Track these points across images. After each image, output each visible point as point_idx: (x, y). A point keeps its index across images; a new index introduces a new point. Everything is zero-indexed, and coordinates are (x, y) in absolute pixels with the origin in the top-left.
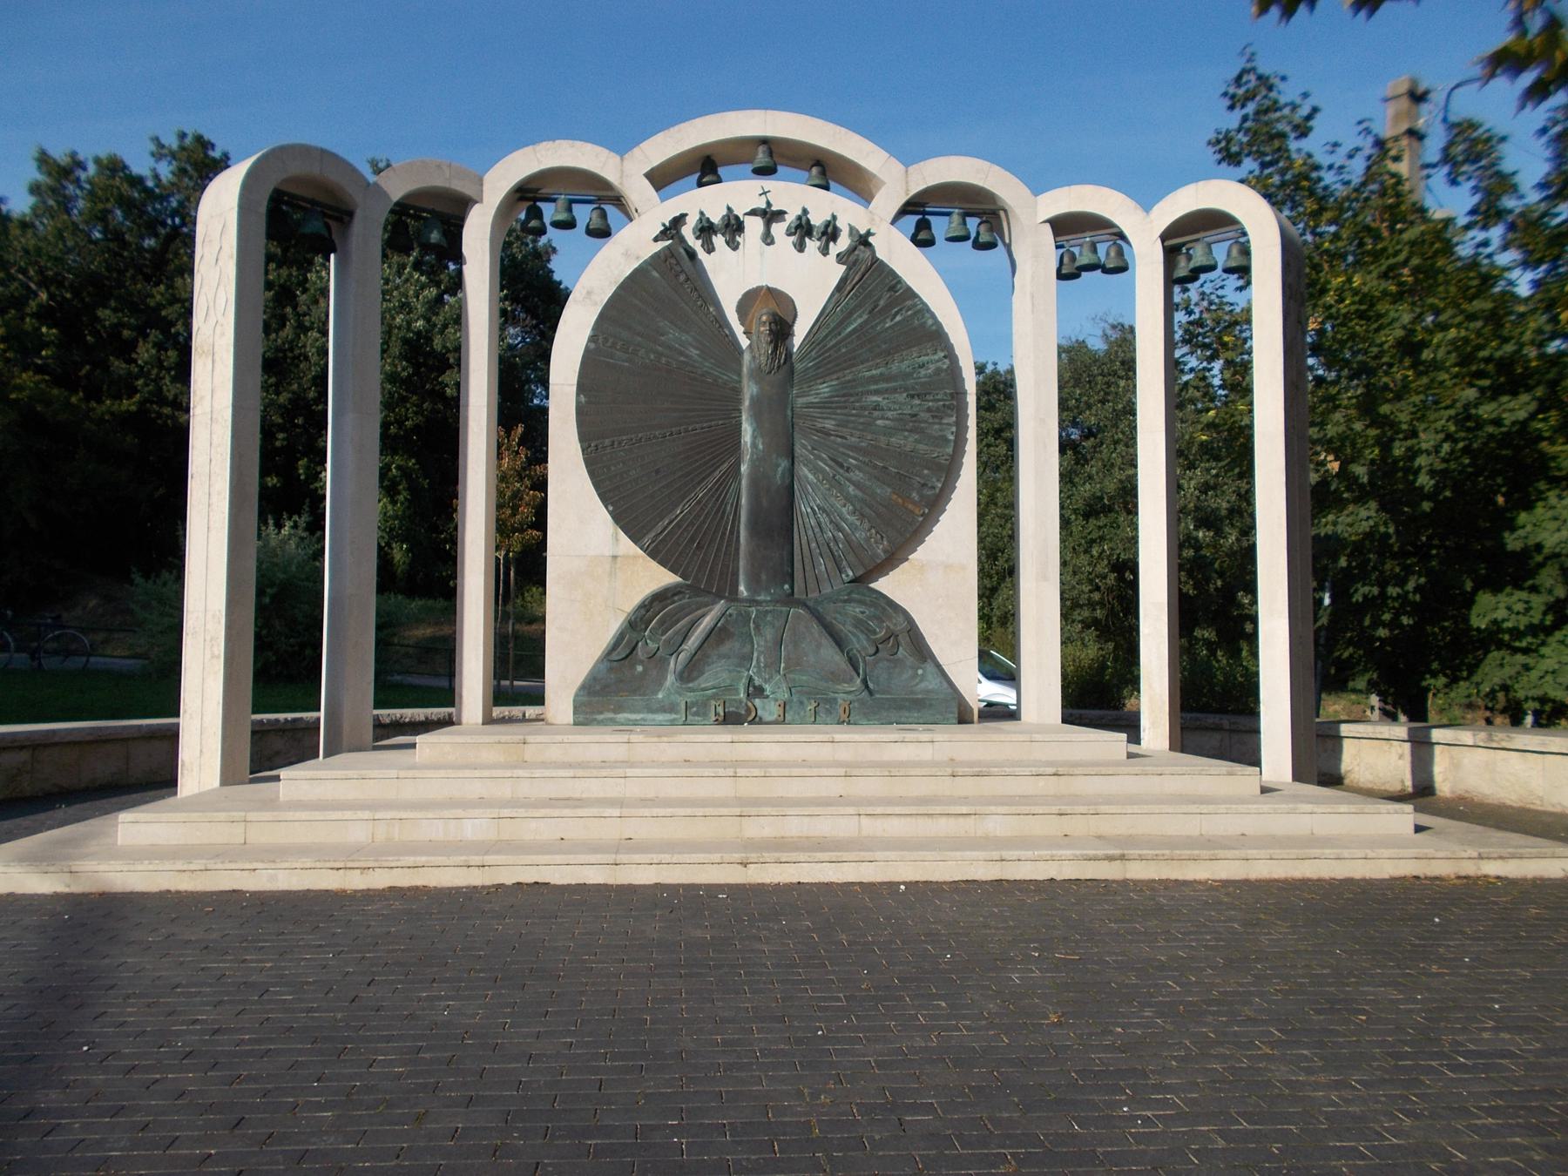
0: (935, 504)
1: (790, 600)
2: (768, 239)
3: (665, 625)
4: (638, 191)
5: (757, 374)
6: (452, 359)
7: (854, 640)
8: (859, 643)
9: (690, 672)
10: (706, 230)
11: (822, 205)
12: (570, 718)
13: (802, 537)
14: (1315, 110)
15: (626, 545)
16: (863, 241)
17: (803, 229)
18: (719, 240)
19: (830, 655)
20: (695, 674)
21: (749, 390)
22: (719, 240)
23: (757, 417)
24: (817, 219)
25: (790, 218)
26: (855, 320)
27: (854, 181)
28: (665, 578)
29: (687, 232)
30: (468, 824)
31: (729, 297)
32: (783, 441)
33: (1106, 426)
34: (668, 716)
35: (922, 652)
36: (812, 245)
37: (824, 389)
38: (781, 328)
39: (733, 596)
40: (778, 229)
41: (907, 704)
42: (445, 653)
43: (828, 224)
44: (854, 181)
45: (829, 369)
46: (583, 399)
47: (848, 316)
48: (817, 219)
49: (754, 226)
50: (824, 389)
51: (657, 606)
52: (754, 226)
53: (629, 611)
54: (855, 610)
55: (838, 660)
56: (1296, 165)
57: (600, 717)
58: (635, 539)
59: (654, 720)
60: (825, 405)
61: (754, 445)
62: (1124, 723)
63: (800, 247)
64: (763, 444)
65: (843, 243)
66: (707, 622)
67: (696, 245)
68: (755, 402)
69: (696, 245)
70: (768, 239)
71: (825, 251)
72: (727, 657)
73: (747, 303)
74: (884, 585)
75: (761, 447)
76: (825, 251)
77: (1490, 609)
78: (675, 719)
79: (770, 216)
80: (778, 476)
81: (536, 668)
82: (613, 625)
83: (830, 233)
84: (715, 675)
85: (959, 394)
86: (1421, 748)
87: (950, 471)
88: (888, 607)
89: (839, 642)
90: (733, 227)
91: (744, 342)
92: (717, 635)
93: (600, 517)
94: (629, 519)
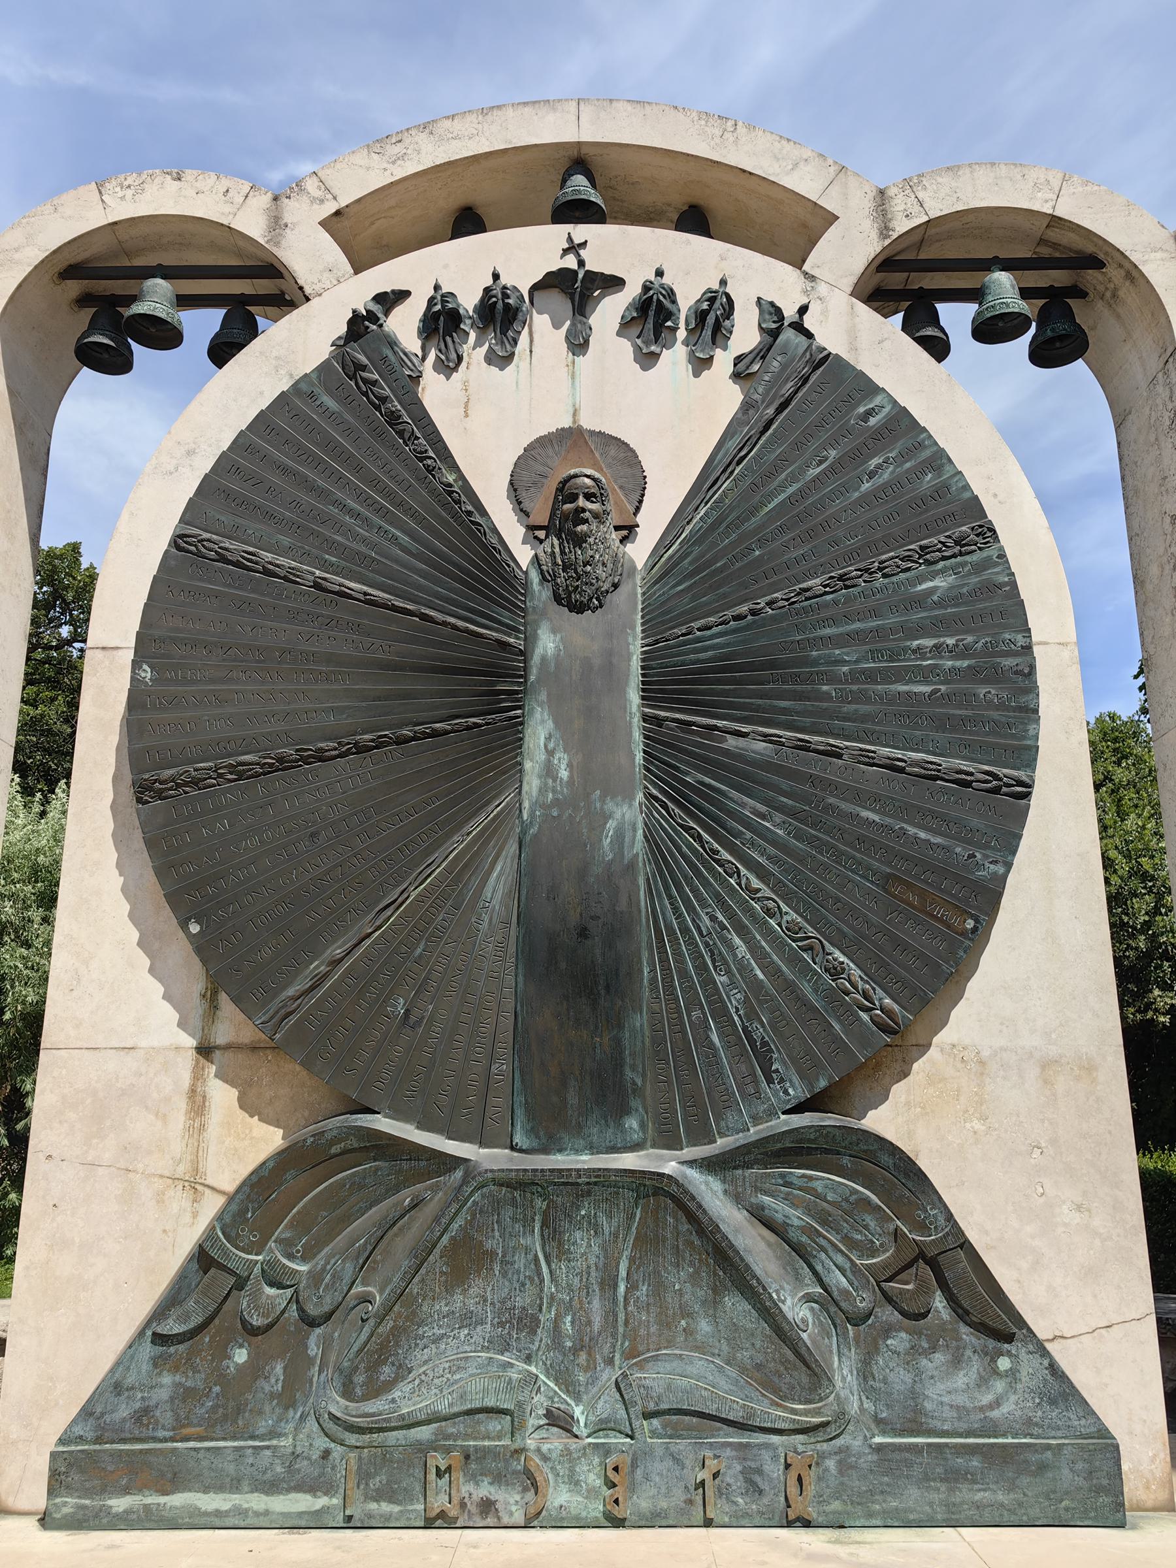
7: (378, 224)
12: (36, 1496)
14: (1136, 677)
20: (387, 1371)
22: (474, 350)
25: (632, 291)
26: (782, 487)
33: (143, 1398)
34: (302, 1502)
41: (975, 1463)
43: (711, 297)
45: (725, 596)
46: (147, 673)
53: (230, 1187)
57: (119, 1504)
59: (267, 1513)
61: (549, 771)
63: (647, 360)
64: (570, 765)
71: (701, 364)
72: (468, 1320)
75: (564, 774)
76: (701, 364)
78: (324, 1510)
80: (606, 842)
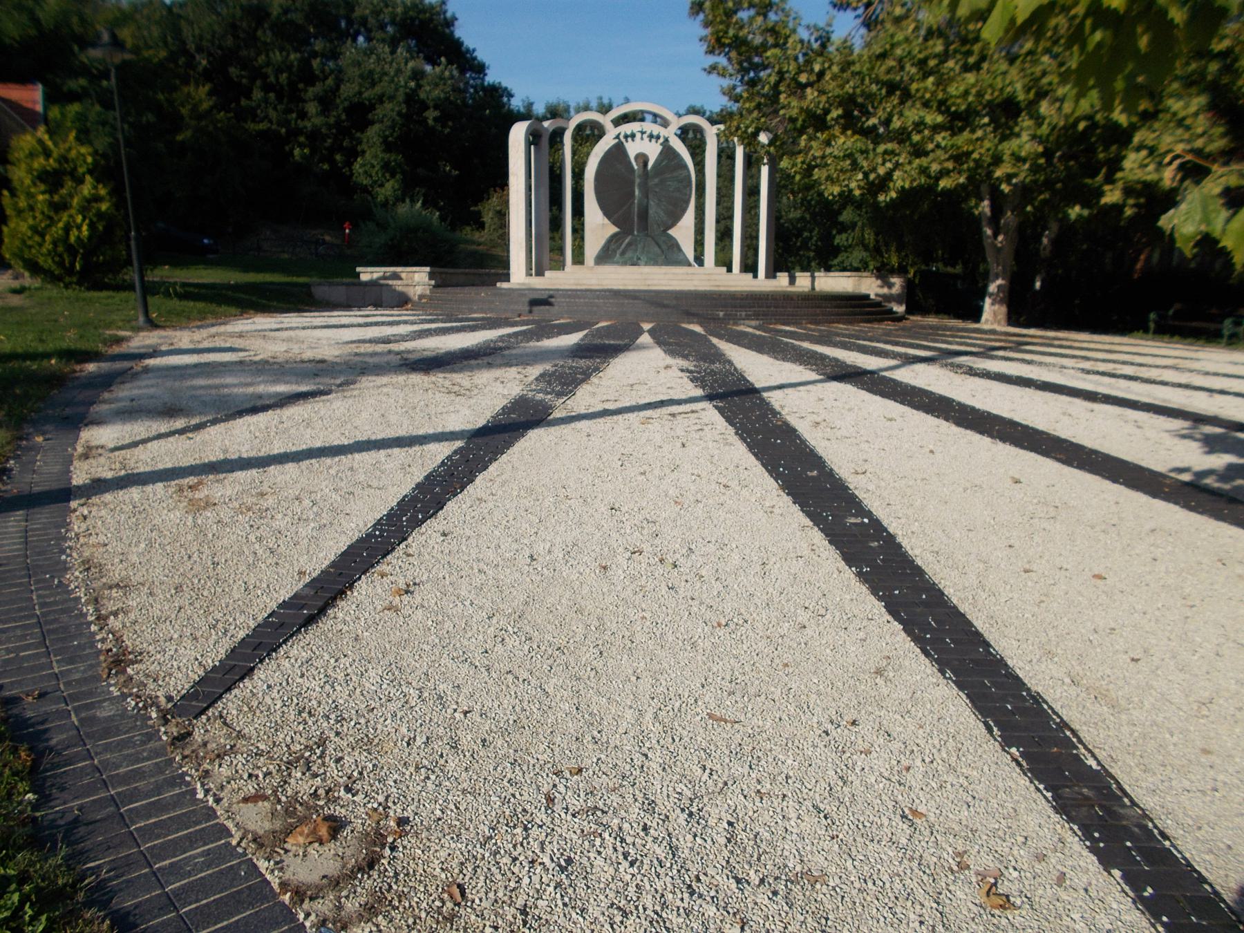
0: (684, 211)
1: (647, 235)
2: (642, 139)
3: (616, 242)
4: (609, 126)
5: (639, 176)
6: (562, 168)
8: (664, 247)
9: (623, 253)
10: (626, 137)
11: (656, 129)
13: (650, 220)
15: (606, 221)
16: (666, 140)
17: (651, 136)
18: (629, 139)
19: (657, 249)
21: (637, 181)
22: (629, 139)
23: (639, 189)
24: (655, 133)
25: (648, 132)
27: (665, 124)
28: (616, 230)
29: (621, 137)
30: (416, 275)
31: (632, 154)
32: (646, 193)
35: (680, 250)
36: (654, 140)
37: (656, 180)
38: (646, 164)
39: (633, 235)
40: (645, 136)
42: (561, 250)
44: (665, 124)
47: (662, 161)
48: (655, 133)
49: (638, 136)
50: (656, 180)
51: (613, 247)
52: (638, 136)
54: (663, 238)
55: (659, 251)
56: (857, 50)
58: (609, 218)
60: (656, 185)
62: (178, 372)
65: (661, 140)
66: (627, 241)
67: (623, 140)
68: (639, 185)
69: (623, 140)
70: (642, 139)
73: (638, 157)
74: (670, 232)
77: (840, 239)
79: (643, 133)
81: (582, 254)
82: (602, 242)
83: (658, 137)
84: (629, 255)
85: (690, 181)
86: (813, 278)
87: (687, 202)
88: (671, 238)
89: (660, 247)
90: (633, 136)
91: (636, 167)
92: (629, 244)
93: (599, 213)
94: (607, 213)
